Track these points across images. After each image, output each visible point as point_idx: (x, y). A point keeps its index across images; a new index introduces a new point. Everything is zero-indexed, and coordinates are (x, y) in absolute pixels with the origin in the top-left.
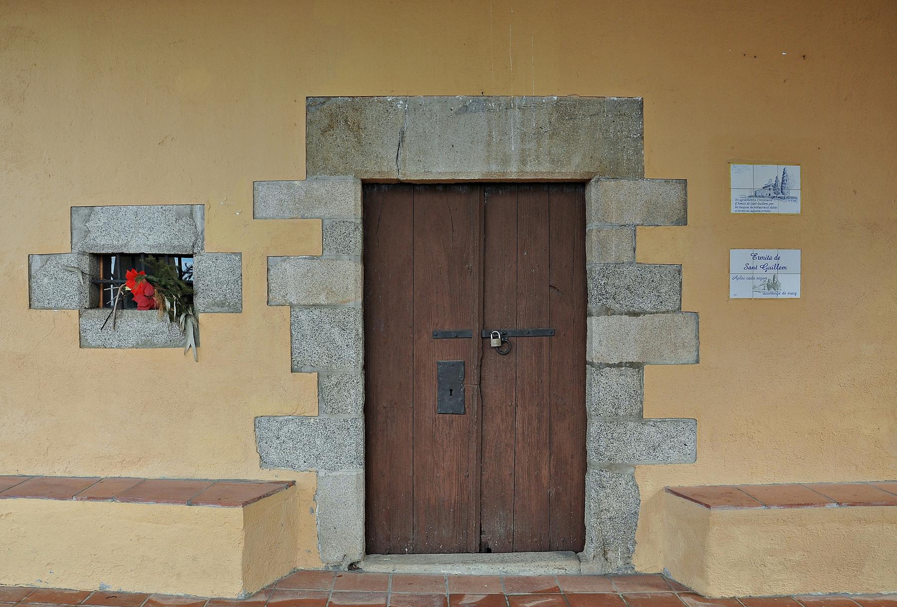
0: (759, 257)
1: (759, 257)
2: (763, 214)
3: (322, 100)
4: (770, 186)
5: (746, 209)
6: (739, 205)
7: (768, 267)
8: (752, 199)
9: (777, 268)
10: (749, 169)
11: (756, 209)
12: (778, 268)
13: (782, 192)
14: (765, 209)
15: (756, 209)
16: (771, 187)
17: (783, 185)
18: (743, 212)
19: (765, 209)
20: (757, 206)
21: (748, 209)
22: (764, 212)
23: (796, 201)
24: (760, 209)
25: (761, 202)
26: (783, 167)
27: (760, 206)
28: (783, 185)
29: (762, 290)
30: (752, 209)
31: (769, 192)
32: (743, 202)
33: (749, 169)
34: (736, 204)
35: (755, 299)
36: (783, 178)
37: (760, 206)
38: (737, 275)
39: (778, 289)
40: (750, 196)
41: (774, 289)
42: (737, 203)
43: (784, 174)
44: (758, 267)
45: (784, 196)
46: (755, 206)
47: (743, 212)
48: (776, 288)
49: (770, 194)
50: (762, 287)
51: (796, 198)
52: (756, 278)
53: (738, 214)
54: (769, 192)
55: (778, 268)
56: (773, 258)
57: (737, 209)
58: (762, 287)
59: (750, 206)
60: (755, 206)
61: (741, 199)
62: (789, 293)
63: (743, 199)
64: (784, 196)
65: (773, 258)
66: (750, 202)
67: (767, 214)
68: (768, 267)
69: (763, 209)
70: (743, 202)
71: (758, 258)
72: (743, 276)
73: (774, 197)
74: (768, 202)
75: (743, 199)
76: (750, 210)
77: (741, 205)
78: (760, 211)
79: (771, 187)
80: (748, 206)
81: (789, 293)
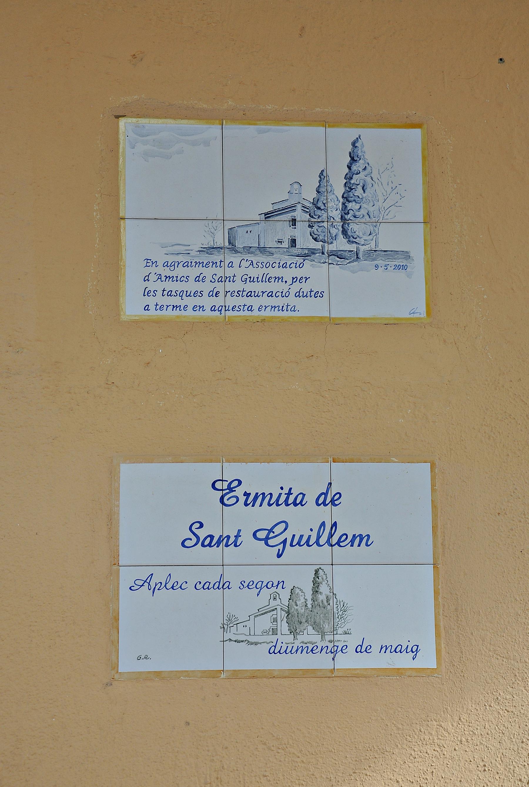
0: (247, 495)
1: (247, 495)
2: (263, 320)
3: (434, 558)
4: (292, 208)
5: (191, 302)
6: (159, 286)
7: (288, 535)
8: (217, 257)
9: (328, 541)
10: (207, 143)
11: (231, 301)
12: (335, 540)
13: (345, 232)
14: (273, 301)
15: (231, 301)
16: (299, 214)
17: (350, 206)
18: (177, 312)
19: (273, 301)
20: (238, 285)
21: (198, 301)
22: (268, 313)
23: (404, 267)
24: (249, 301)
25: (253, 272)
26: (352, 133)
27: (249, 287)
28: (350, 206)
29: (265, 633)
30: (218, 301)
31: (288, 232)
32: (180, 271)
33: (207, 143)
34: (146, 279)
35: (236, 674)
36: (349, 178)
37: (249, 287)
38: (150, 570)
39: (334, 632)
40: (210, 250)
41: (318, 628)
42: (153, 277)
43: (353, 160)
44: (246, 537)
45: (353, 247)
46: (230, 287)
47: (285, 314)
48: (327, 627)
49: (293, 242)
50: (265, 622)
51: (407, 255)
52: (235, 584)
53: (158, 322)
54: (288, 232)
55: (335, 540)
56: (310, 499)
57: (151, 301)
58: (265, 622)
59: (206, 287)
60: (230, 287)
61: (171, 259)
62: (384, 648)
63: (180, 258)
64: (353, 247)
65: (310, 499)
66: (208, 272)
67: (283, 320)
68: (288, 535)
69: (265, 300)
70: (180, 271)
71: (242, 499)
72: (178, 575)
73: (313, 252)
74: (288, 274)
75: (180, 258)
76: (207, 302)
77: (170, 286)
78: (250, 309)
79: (299, 214)
80: (199, 287)
81: (384, 648)
